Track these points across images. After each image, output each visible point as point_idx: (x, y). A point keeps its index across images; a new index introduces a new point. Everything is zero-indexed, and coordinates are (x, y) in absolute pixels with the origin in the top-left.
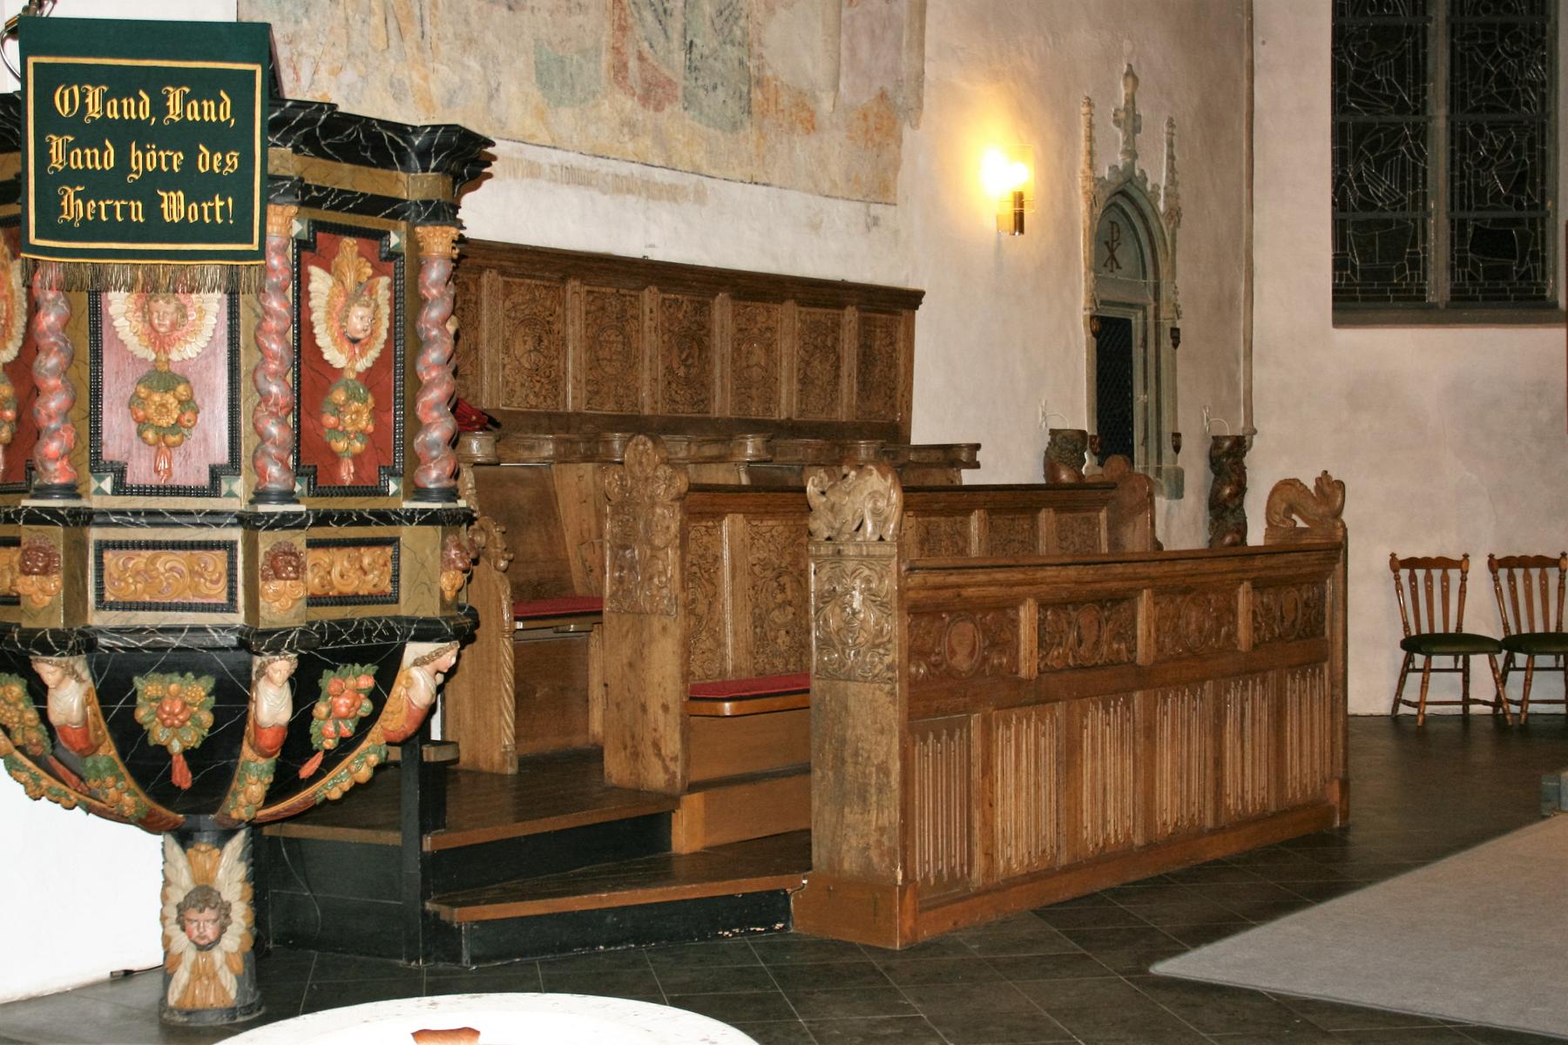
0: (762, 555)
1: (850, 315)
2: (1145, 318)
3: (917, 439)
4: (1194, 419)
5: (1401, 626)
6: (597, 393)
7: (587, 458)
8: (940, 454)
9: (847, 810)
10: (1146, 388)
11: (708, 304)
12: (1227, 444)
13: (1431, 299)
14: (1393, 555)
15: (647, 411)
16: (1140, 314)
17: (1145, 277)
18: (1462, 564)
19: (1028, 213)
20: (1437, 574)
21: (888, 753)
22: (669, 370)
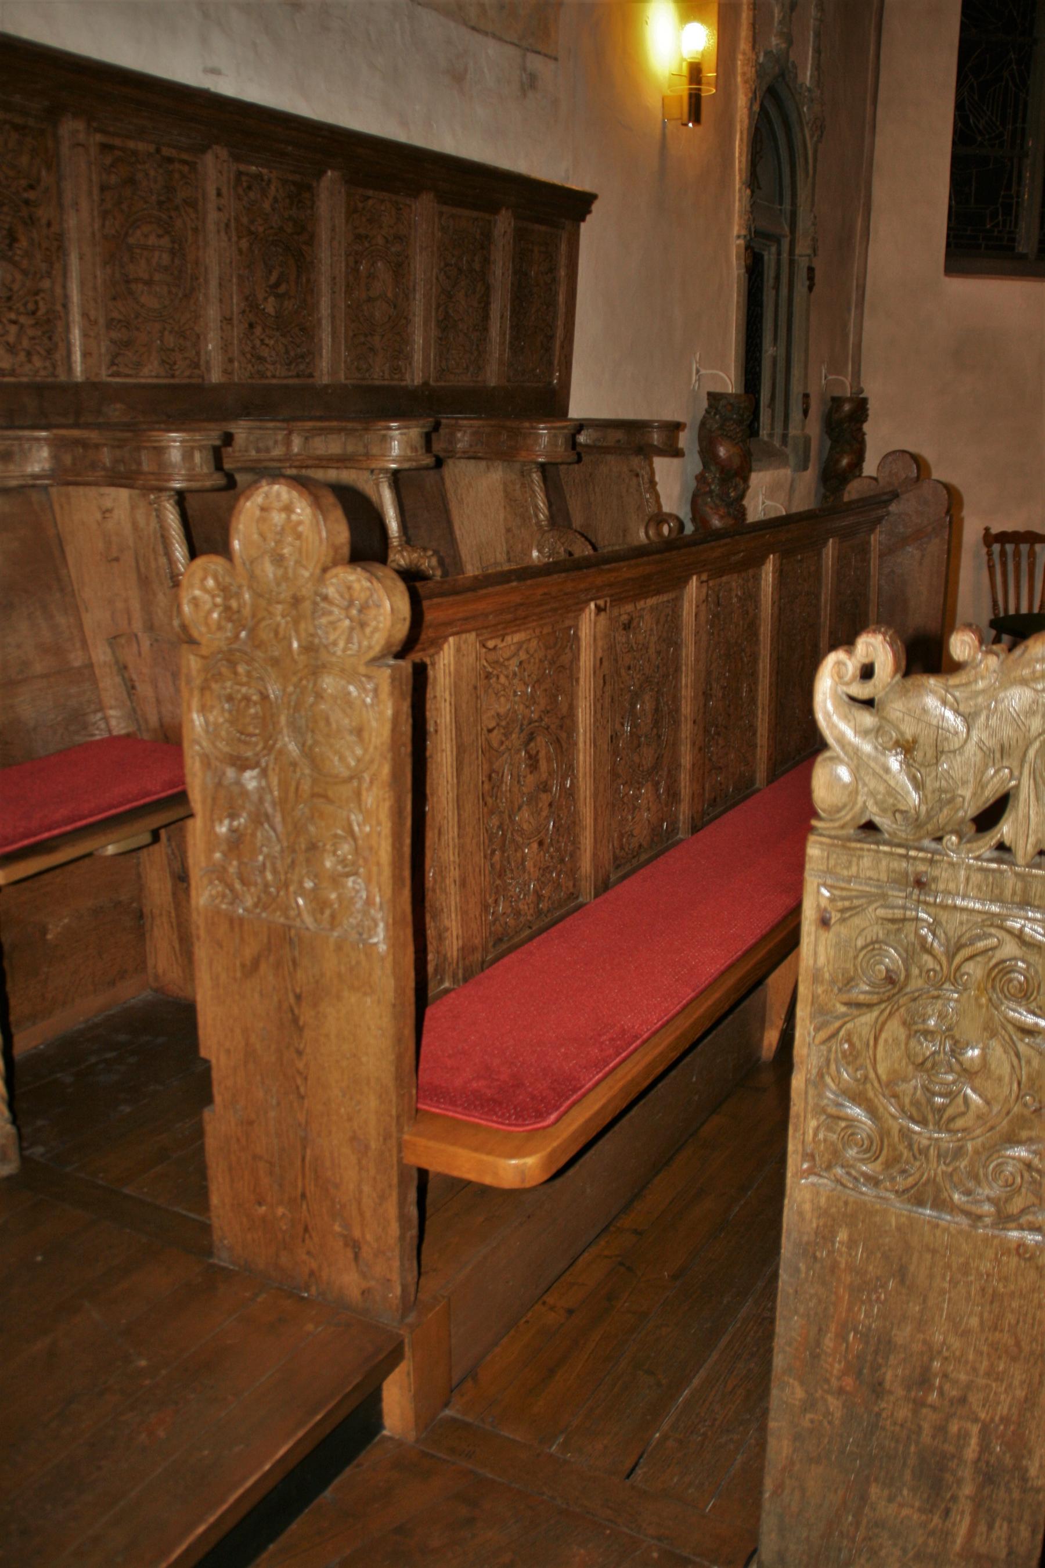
0: (502, 707)
1: (503, 224)
2: (779, 253)
4: (817, 379)
5: (991, 604)
6: (128, 344)
7: (119, 479)
8: (619, 435)
9: (874, 1490)
10: (775, 339)
11: (309, 188)
12: (847, 407)
14: (987, 529)
15: (215, 377)
16: (774, 249)
17: (781, 204)
19: (709, 91)
20: (1024, 548)
22: (251, 304)
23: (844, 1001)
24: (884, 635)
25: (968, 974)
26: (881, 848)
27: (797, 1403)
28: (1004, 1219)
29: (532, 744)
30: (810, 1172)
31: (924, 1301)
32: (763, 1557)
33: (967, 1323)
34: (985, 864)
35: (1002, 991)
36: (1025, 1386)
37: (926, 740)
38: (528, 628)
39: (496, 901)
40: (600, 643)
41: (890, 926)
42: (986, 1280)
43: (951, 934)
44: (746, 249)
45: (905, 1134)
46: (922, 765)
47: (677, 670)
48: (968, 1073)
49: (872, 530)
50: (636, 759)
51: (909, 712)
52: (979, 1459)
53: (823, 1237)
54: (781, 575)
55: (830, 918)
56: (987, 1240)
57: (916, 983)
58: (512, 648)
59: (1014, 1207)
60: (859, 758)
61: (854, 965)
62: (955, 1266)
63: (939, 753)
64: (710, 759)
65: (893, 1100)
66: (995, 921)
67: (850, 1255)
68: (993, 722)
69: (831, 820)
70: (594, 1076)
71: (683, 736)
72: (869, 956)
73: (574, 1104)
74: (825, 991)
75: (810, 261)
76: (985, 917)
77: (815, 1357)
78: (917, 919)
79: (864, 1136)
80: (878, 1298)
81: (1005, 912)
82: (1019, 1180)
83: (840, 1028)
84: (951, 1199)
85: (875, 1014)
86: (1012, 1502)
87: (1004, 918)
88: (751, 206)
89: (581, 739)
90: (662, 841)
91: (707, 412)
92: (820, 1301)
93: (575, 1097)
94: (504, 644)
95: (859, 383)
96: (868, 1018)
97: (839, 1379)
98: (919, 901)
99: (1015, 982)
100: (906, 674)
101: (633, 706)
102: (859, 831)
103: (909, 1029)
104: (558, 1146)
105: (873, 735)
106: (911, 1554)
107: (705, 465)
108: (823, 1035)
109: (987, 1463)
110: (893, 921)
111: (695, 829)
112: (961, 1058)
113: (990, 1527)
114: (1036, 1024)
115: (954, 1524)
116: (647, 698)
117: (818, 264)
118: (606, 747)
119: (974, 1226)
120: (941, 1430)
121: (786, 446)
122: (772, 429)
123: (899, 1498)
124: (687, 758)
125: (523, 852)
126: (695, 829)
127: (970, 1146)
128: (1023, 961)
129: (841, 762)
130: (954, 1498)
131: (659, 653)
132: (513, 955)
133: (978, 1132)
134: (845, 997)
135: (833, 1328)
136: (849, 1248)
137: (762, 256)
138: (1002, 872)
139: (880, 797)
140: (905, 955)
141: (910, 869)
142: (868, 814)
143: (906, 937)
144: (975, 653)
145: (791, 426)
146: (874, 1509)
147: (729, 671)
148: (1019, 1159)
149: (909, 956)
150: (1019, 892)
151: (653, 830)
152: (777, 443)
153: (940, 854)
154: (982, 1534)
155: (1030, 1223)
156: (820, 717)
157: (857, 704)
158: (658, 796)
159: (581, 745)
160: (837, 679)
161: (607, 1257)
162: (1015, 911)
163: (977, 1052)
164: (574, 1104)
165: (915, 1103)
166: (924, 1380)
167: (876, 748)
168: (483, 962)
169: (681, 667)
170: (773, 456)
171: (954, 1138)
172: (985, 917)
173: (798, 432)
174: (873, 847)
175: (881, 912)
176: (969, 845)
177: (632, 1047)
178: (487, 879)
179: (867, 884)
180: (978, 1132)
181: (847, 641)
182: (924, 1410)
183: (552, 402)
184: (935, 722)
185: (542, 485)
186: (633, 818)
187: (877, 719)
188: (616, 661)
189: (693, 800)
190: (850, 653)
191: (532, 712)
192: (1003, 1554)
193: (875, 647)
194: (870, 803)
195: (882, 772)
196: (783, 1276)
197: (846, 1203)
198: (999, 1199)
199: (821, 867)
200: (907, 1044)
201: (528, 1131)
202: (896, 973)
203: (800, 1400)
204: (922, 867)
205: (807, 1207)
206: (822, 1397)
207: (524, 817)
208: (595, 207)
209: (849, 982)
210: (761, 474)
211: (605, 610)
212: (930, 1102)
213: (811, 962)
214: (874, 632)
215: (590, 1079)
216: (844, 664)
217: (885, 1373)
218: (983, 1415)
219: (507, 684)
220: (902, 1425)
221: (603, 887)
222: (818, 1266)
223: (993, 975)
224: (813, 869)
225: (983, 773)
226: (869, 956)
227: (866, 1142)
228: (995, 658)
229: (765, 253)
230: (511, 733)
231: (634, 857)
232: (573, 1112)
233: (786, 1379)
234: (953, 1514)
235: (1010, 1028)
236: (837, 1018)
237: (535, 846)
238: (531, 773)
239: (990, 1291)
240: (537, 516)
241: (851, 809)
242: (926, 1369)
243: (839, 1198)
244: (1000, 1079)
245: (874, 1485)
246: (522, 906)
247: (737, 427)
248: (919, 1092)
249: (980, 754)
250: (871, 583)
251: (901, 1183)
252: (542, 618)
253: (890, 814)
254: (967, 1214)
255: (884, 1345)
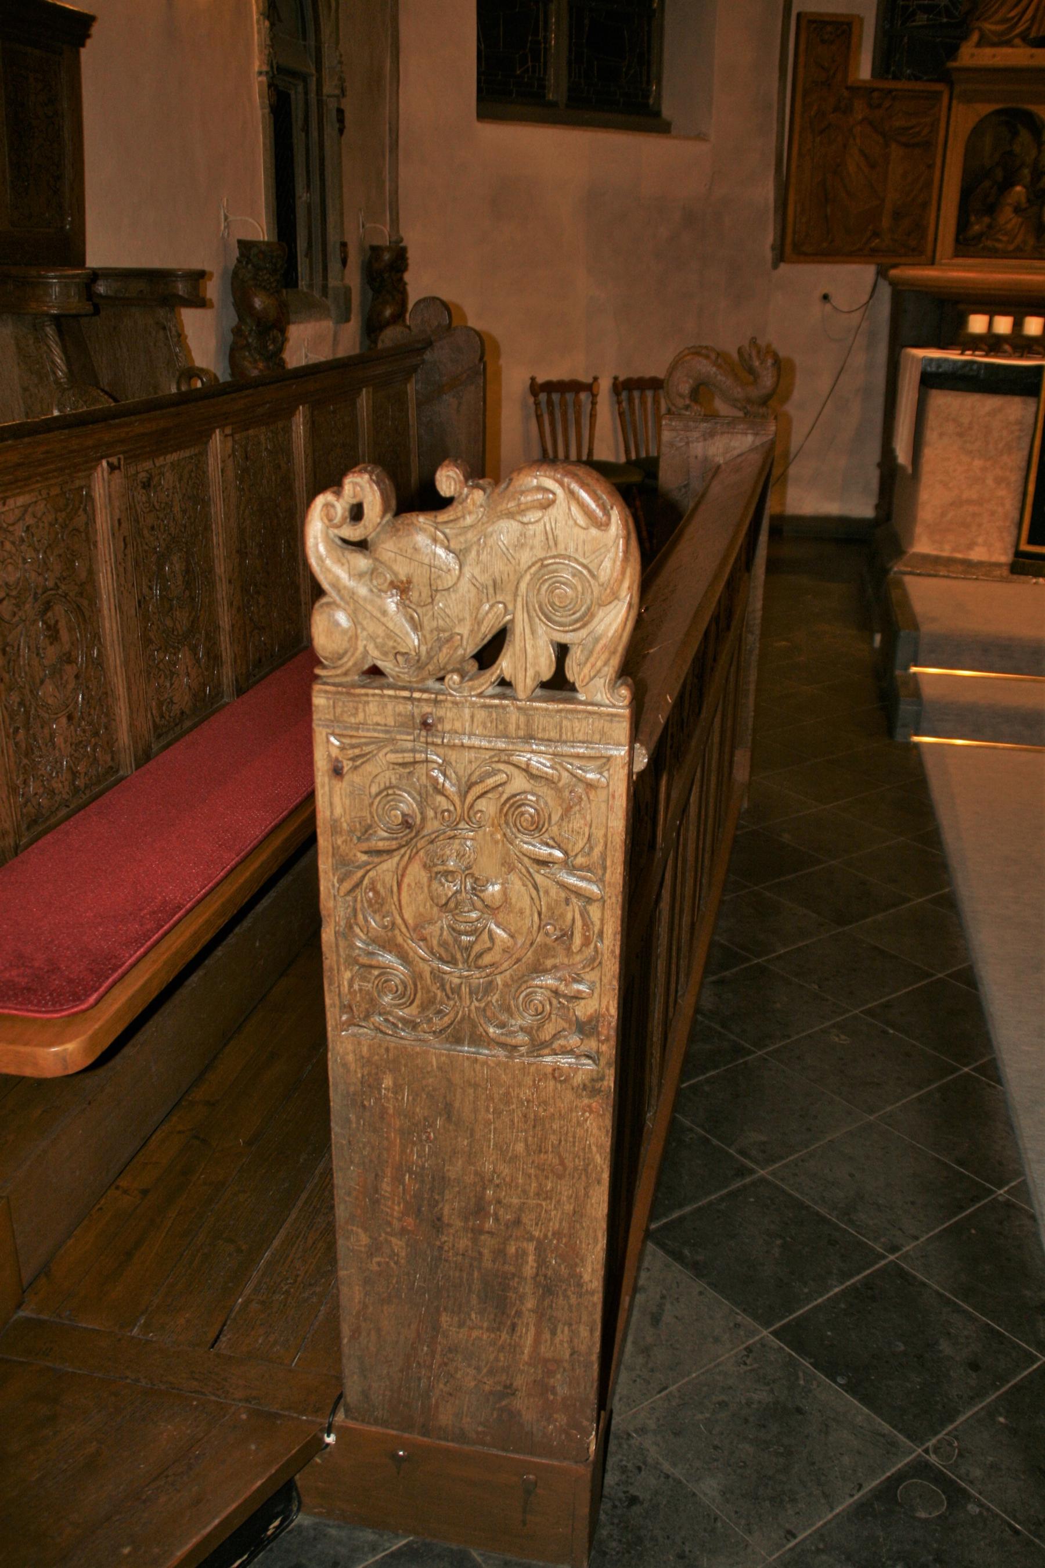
2: (306, 93)
3: (94, 260)
4: (355, 228)
9: (445, 1319)
12: (387, 256)
13: (550, 96)
14: (533, 379)
16: (300, 89)
17: (305, 39)
18: (590, 388)
20: (569, 397)
21: (578, 1213)
23: (363, 850)
24: (371, 473)
25: (481, 811)
26: (386, 692)
27: (363, 1249)
28: (538, 1047)
29: (50, 614)
30: (350, 1023)
31: (472, 1135)
32: (349, 1399)
33: (513, 1150)
34: (488, 701)
35: (515, 825)
36: (572, 1200)
37: (420, 579)
38: (32, 490)
39: (25, 782)
40: (117, 504)
41: (401, 770)
42: (527, 1107)
43: (461, 773)
44: (270, 86)
45: (437, 976)
46: (419, 605)
47: (207, 528)
48: (490, 909)
49: (407, 380)
50: (169, 623)
51: (401, 553)
52: (537, 1274)
53: (369, 1086)
54: (314, 428)
55: (342, 768)
56: (524, 1069)
57: (433, 825)
58: (17, 511)
59: (547, 1033)
60: (356, 602)
61: (371, 813)
62: (496, 1096)
63: (434, 592)
64: (251, 619)
65: (421, 943)
66: (503, 757)
67: (397, 1099)
68: (484, 557)
69: (334, 668)
70: (136, 952)
71: (219, 597)
72: (384, 801)
73: (115, 983)
74: (345, 841)
75: (339, 102)
76: (492, 753)
77: (376, 1202)
78: (427, 761)
79: (398, 981)
80: (428, 1138)
81: (511, 747)
82: (548, 1007)
83: (364, 877)
84: (487, 1033)
85: (396, 859)
86: (570, 1306)
87: (509, 753)
88: (272, 40)
89: (105, 606)
90: (205, 705)
91: (239, 261)
92: (373, 1148)
93: (116, 975)
94: (6, 508)
95: (398, 231)
96: (390, 864)
97: (400, 1220)
98: (427, 743)
99: (527, 816)
100: (397, 514)
101: (161, 568)
102: (364, 677)
103: (430, 872)
104: (100, 1028)
105: (367, 577)
106: (485, 1370)
107: (241, 318)
108: (347, 885)
109: (545, 1276)
110: (404, 765)
111: (240, 691)
112: (481, 895)
113: (554, 1333)
114: (550, 854)
115: (520, 1337)
116: (175, 559)
117: (347, 105)
118: (133, 612)
119: (511, 1057)
120: (500, 1253)
121: (327, 297)
122: (311, 279)
123: (468, 1323)
124: (225, 619)
125: (51, 728)
126: (240, 691)
127: (499, 980)
128: (533, 794)
129: (338, 606)
130: (519, 1314)
131: (184, 512)
132: (49, 836)
133: (505, 965)
134: (365, 846)
135: (389, 1171)
136: (396, 1093)
137: (289, 95)
138: (504, 707)
139: (379, 640)
140: (418, 798)
141: (416, 711)
142: (370, 658)
143: (418, 780)
144: (462, 488)
145: (330, 275)
146: (446, 1336)
147: (264, 528)
148: (547, 988)
149: (423, 801)
150: (522, 726)
151: (194, 695)
152: (317, 294)
153: (443, 694)
154: (546, 1341)
155: (562, 1047)
156: (313, 561)
157: (350, 547)
158: (198, 661)
159: (106, 612)
160: (326, 521)
161: (179, 1132)
162: (520, 746)
163: (497, 887)
164: (115, 983)
165: (443, 944)
166: (479, 1209)
167: (371, 591)
168: (17, 847)
169: (211, 525)
170: (312, 308)
171: (484, 974)
172: (492, 753)
173: (338, 283)
174: (377, 691)
175: (392, 757)
176: (470, 683)
177: (175, 918)
178: (12, 759)
179: (375, 730)
180: (505, 965)
181: (334, 483)
182: (483, 1237)
183: (68, 248)
184: (426, 561)
185: (57, 338)
186: (172, 685)
187: (371, 561)
188: (137, 521)
189: (235, 662)
190: (338, 494)
191: (46, 580)
192: (567, 1356)
193: (362, 487)
194: (371, 648)
195: (379, 615)
196: (336, 1128)
197: (387, 1050)
198: (532, 1028)
199: (327, 716)
200: (429, 886)
201: (69, 1016)
202: (412, 817)
203: (366, 1245)
204: (427, 709)
205: (351, 1058)
206: (386, 1240)
207: (48, 690)
208: (95, 30)
209: (367, 830)
210: (302, 327)
211: (119, 468)
212: (457, 941)
213: (328, 813)
214: (360, 471)
215: (131, 956)
216: (333, 506)
217: (442, 1209)
218: (537, 1234)
219: (14, 550)
220: (463, 1255)
221: (144, 757)
222: (368, 1114)
223: (505, 810)
224: (320, 720)
225: (478, 609)
226: (384, 801)
227: (400, 987)
228: (481, 492)
229: (292, 93)
230: (24, 603)
231: (176, 725)
232: (115, 991)
233: (350, 1227)
234: (519, 1328)
235: (526, 860)
236: (359, 867)
237: (64, 720)
238: (51, 644)
239: (532, 1116)
240: (55, 373)
241: (353, 654)
242: (480, 1198)
243: (380, 1046)
244: (521, 912)
245: (444, 1314)
246: (56, 785)
247: (272, 276)
248: (445, 933)
249: (473, 590)
250: (411, 433)
251: (438, 1023)
252: (47, 479)
253: (391, 657)
254: (503, 1045)
255: (440, 1182)
